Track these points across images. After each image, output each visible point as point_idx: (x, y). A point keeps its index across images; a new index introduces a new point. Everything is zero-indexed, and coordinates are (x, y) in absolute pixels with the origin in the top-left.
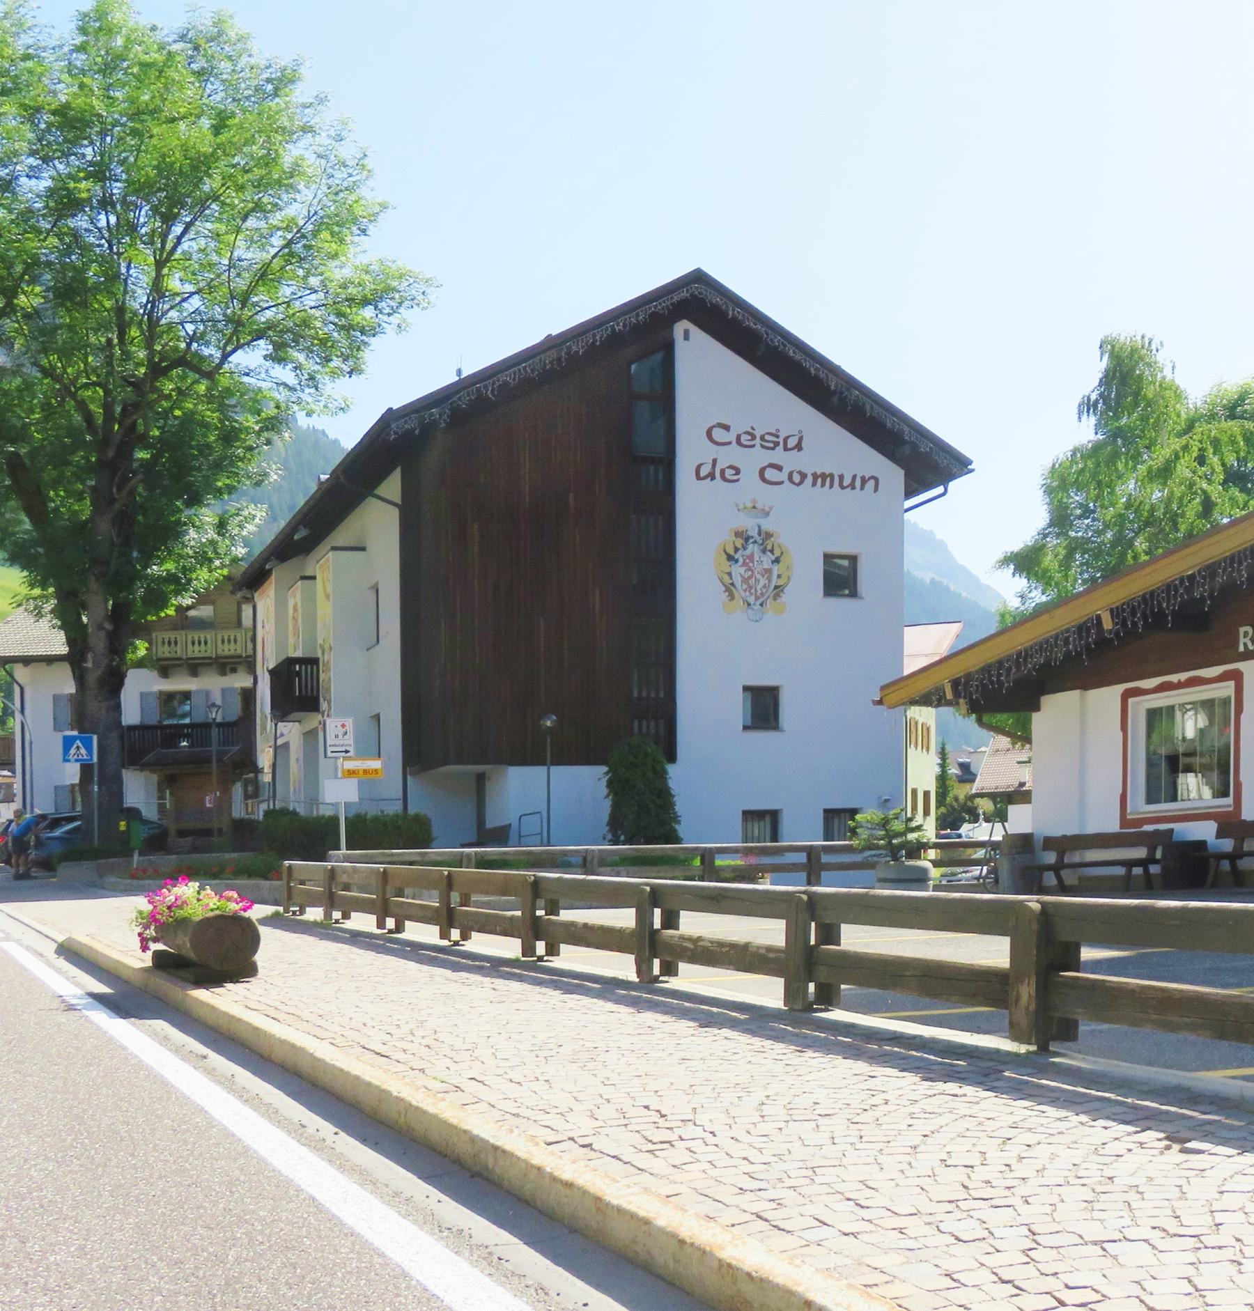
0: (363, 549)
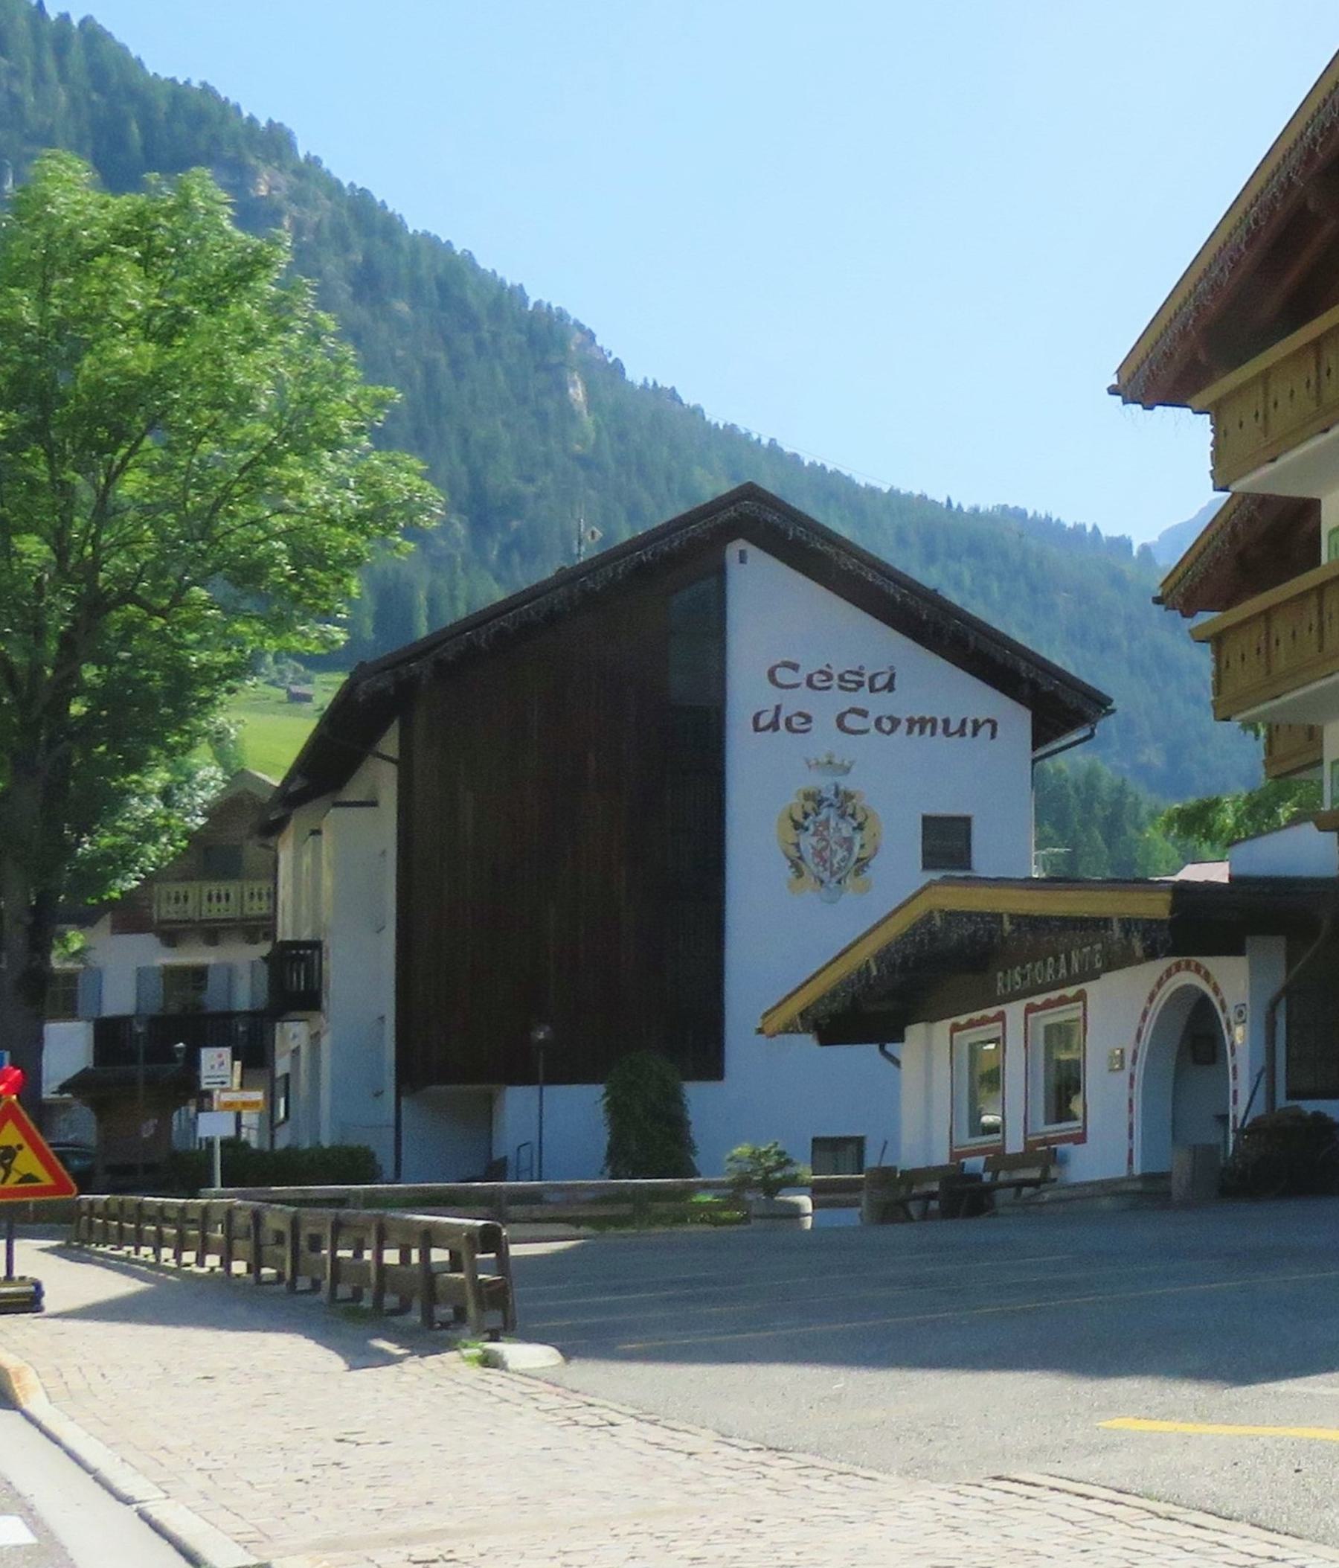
0: (374, 804)
